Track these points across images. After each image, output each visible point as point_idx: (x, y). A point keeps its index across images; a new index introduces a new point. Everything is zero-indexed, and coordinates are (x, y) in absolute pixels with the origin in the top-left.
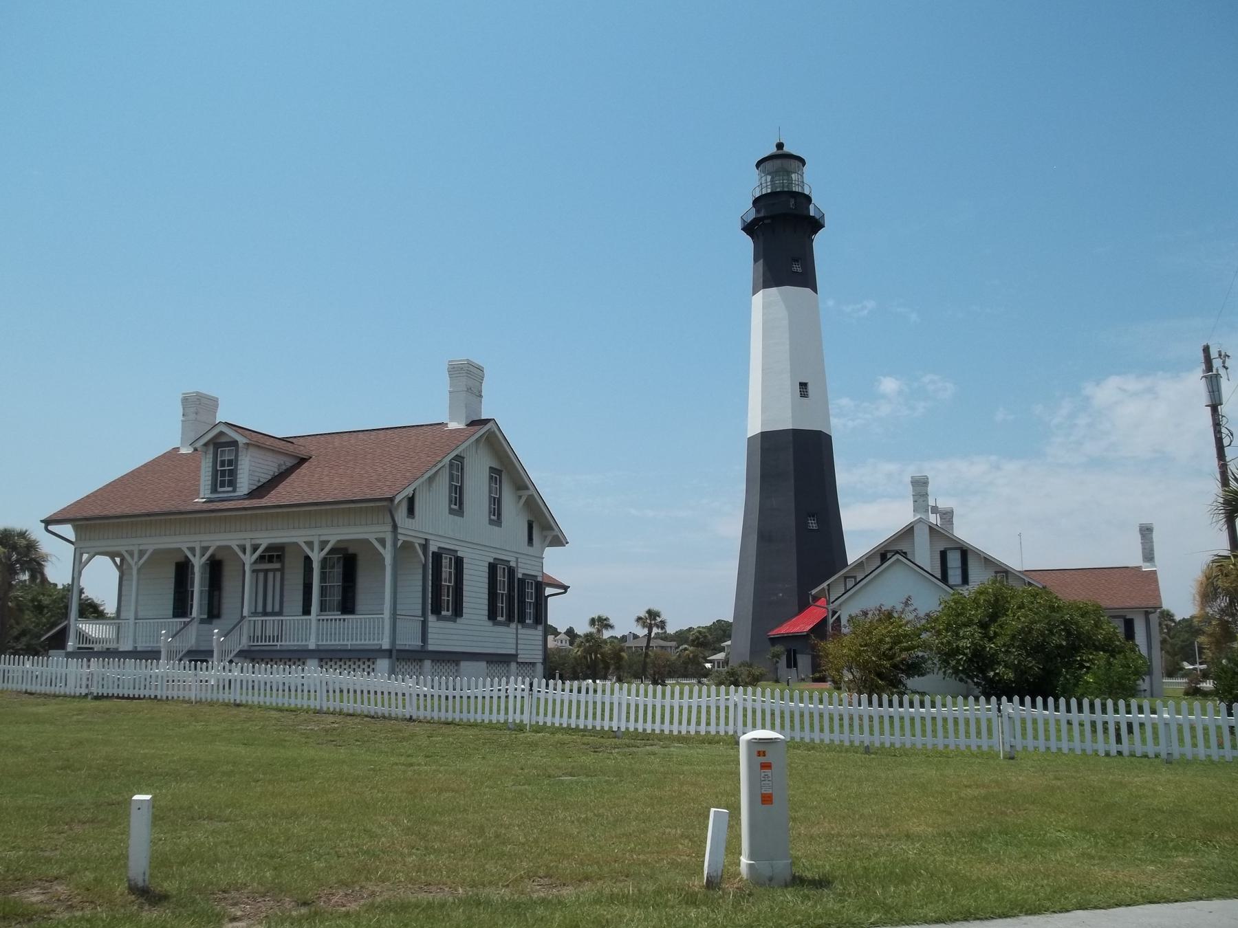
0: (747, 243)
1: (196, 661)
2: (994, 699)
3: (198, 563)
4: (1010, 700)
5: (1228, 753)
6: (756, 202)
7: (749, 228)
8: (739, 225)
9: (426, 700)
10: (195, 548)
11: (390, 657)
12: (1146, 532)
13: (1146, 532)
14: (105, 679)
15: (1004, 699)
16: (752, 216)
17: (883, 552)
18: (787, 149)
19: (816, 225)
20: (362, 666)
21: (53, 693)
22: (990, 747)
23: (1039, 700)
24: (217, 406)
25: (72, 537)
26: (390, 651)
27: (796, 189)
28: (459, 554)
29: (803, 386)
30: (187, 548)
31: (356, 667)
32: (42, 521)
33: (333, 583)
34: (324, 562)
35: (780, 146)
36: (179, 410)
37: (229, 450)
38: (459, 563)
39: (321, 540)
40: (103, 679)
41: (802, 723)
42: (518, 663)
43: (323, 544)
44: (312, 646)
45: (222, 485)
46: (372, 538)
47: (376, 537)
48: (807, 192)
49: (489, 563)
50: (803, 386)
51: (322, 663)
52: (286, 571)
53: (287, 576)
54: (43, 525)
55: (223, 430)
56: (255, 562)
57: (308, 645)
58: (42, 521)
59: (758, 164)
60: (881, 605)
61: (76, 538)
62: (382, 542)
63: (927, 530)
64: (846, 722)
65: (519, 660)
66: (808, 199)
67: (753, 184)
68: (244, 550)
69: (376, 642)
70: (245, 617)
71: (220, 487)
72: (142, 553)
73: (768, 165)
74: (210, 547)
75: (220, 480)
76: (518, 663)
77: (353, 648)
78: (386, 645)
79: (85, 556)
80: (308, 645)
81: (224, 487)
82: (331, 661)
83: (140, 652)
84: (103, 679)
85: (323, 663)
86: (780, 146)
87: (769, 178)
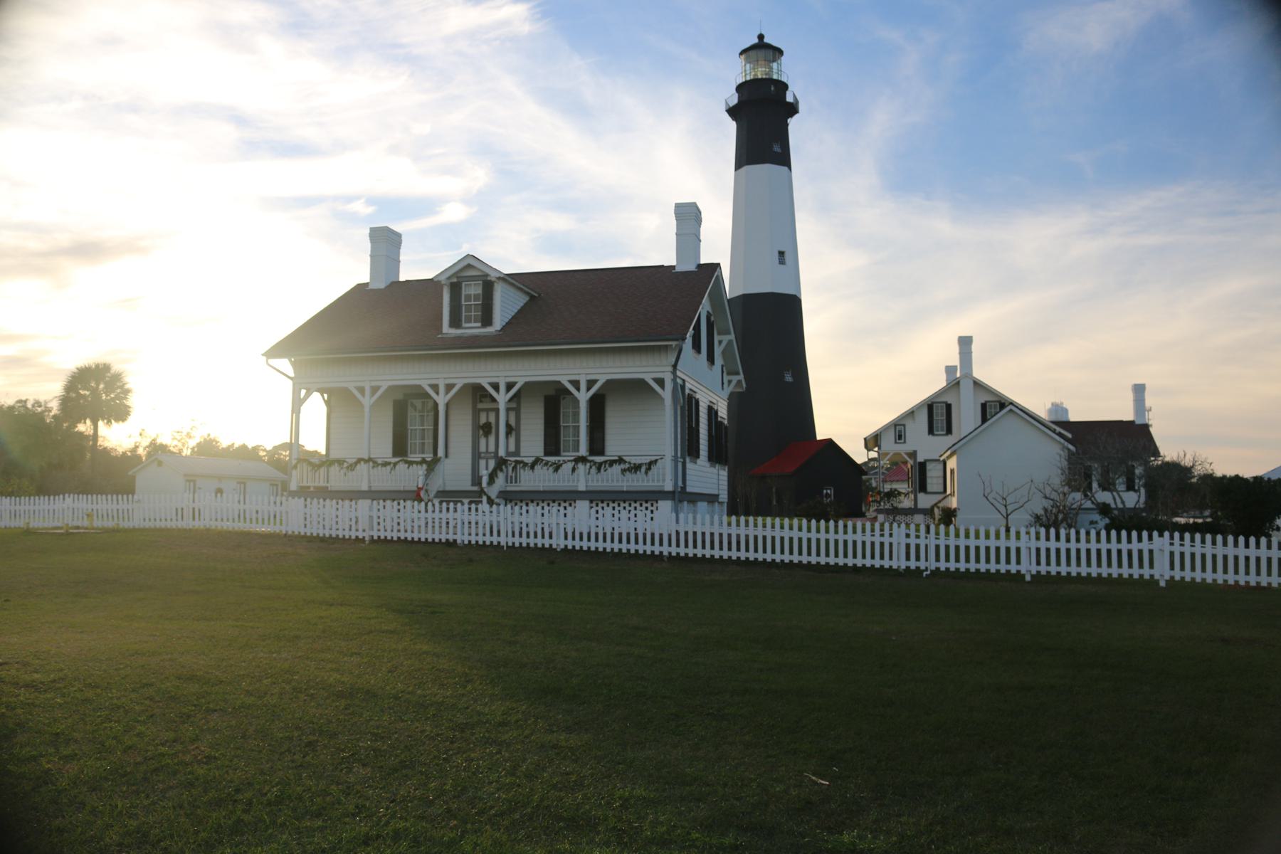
0: (732, 126)
1: (448, 502)
2: (1167, 534)
3: (583, 397)
4: (1161, 535)
5: (1275, 581)
6: (740, 88)
7: (732, 112)
8: (724, 108)
9: (470, 527)
10: (498, 383)
11: (673, 499)
12: (1139, 390)
13: (1139, 390)
14: (381, 524)
15: (1155, 534)
16: (734, 100)
17: (930, 403)
18: (766, 40)
19: (793, 109)
20: (628, 508)
21: (284, 532)
22: (1246, 582)
23: (1252, 540)
24: (400, 243)
25: (292, 375)
26: (673, 493)
27: (775, 77)
28: (697, 396)
29: (781, 254)
30: (355, 387)
31: (621, 508)
32: (263, 355)
33: (415, 426)
34: (447, 405)
35: (761, 37)
36: (367, 245)
37: (475, 284)
38: (697, 402)
39: (588, 379)
40: (399, 524)
41: (1247, 566)
42: (719, 503)
43: (591, 384)
44: (582, 488)
45: (468, 320)
46: (648, 378)
47: (569, 379)
48: (784, 79)
49: (709, 406)
50: (781, 254)
51: (592, 505)
52: (523, 410)
53: (523, 416)
54: (265, 358)
55: (471, 263)
56: (511, 400)
57: (663, 486)
58: (263, 355)
59: (741, 54)
60: (136, 443)
61: (295, 373)
62: (661, 382)
63: (972, 383)
64: (266, 521)
65: (720, 500)
66: (783, 87)
67: (737, 72)
68: (362, 390)
69: (620, 484)
70: (440, 458)
71: (465, 322)
72: (452, 386)
73: (752, 53)
74: (381, 387)
75: (465, 316)
76: (719, 503)
77: (546, 489)
78: (669, 487)
79: (303, 392)
80: (663, 486)
81: (470, 322)
82: (635, 502)
83: (331, 491)
84: (399, 524)
85: (594, 505)
86: (761, 37)
87: (752, 66)
